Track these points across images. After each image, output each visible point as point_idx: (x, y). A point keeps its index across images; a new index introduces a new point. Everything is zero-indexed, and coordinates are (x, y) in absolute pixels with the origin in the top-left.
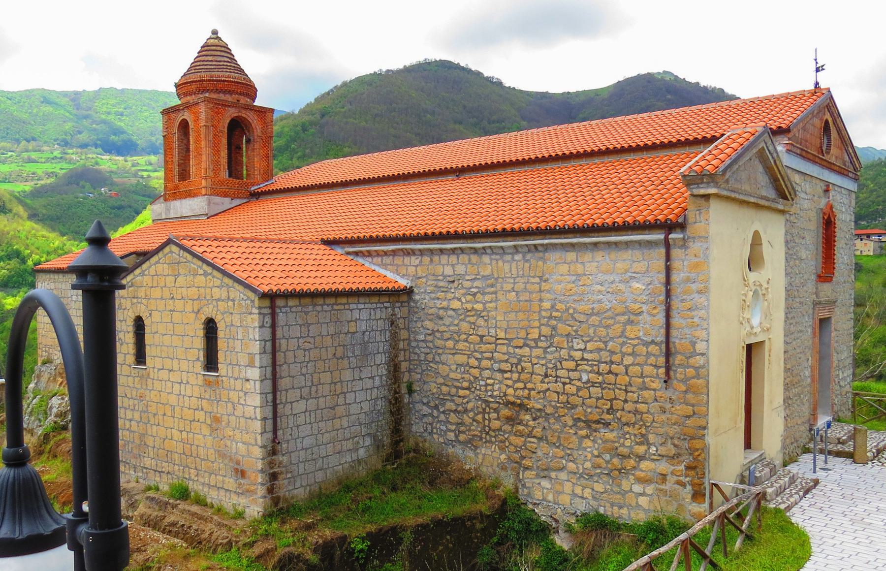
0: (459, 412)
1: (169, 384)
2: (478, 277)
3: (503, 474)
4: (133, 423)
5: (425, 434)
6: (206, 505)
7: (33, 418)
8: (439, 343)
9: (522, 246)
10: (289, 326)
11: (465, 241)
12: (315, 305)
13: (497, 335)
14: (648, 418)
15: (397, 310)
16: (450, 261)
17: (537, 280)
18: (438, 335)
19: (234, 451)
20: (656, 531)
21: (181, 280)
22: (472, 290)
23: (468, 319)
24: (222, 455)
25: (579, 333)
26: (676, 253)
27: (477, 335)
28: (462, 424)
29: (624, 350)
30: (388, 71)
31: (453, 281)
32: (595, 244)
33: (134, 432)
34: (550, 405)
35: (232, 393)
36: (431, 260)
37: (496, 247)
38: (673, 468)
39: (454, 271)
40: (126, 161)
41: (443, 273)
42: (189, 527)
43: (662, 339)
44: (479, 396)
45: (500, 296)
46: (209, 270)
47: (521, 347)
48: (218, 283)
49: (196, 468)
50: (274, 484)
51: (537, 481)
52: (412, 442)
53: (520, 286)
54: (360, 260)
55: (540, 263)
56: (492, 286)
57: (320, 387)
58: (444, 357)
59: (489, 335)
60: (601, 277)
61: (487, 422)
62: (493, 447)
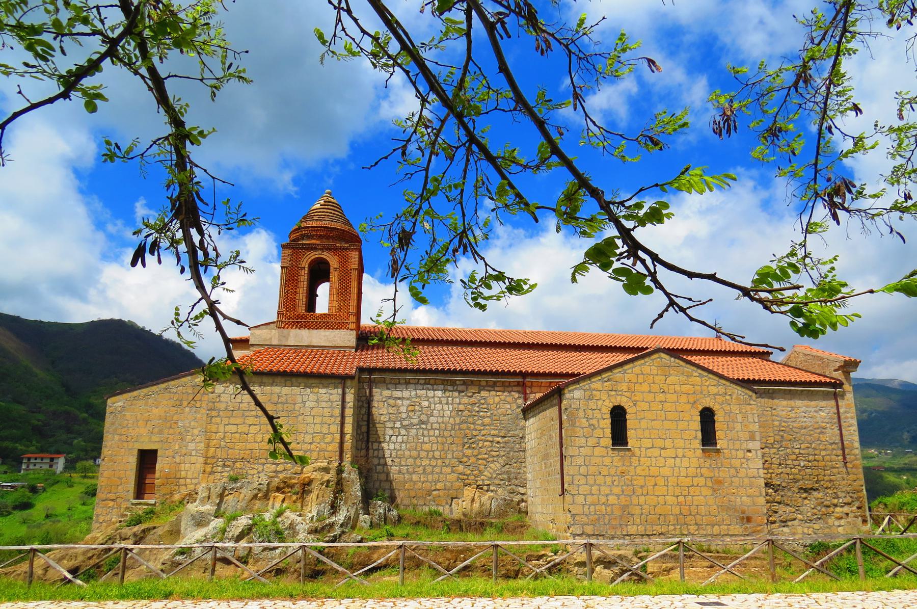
4: (610, 498)
14: (837, 483)
24: (728, 508)
35: (733, 461)
49: (696, 524)
51: (781, 529)
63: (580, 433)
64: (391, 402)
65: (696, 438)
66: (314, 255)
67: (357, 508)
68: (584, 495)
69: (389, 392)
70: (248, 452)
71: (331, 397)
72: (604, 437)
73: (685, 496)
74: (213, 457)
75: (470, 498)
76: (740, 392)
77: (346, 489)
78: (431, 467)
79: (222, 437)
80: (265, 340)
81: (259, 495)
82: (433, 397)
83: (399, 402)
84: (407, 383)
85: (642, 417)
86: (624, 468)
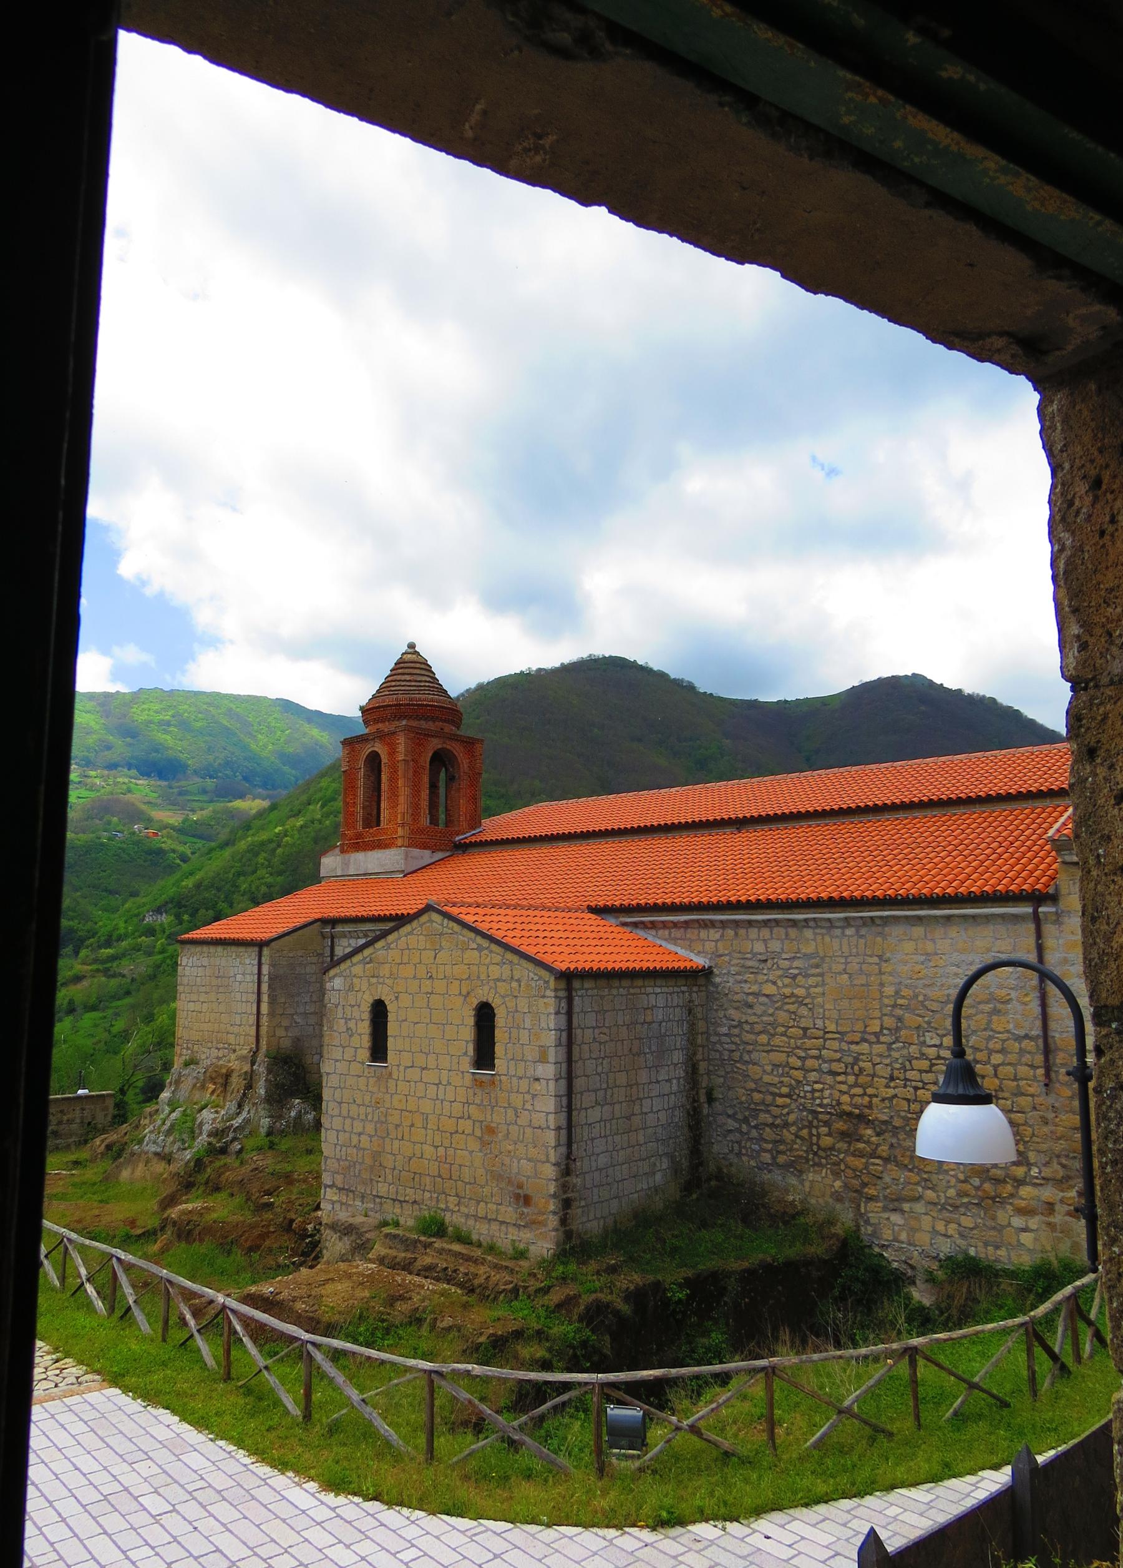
0: (777, 1126)
1: (421, 1086)
2: (798, 955)
3: (838, 1206)
4: (363, 1137)
5: (731, 1156)
6: (471, 1243)
7: (171, 1138)
8: (750, 1037)
9: (854, 918)
10: (586, 1013)
11: (780, 911)
12: (611, 987)
13: (826, 1028)
15: (694, 995)
16: (761, 935)
17: (876, 960)
18: (747, 1027)
19: (515, 1170)
20: (1046, 1277)
21: (443, 956)
23: (787, 1007)
25: (932, 1025)
26: (1049, 929)
27: (799, 1027)
28: (782, 1141)
29: (991, 1045)
30: (540, 670)
31: (766, 961)
32: (948, 918)
33: (364, 1149)
34: (899, 1116)
35: (513, 1096)
36: (736, 934)
37: (821, 919)
38: (1062, 1194)
39: (766, 948)
40: (171, 788)
41: (752, 950)
42: (455, 1271)
43: (1037, 1033)
44: (803, 1105)
45: (828, 980)
46: (485, 943)
47: (857, 1043)
48: (498, 959)
49: (457, 1195)
50: (567, 1213)
51: (886, 1215)
52: (712, 1167)
53: (854, 966)
54: (641, 933)
55: (879, 939)
56: (817, 966)
57: (616, 1090)
58: (755, 1055)
59: (815, 1028)
60: (956, 957)
61: (815, 1139)
62: (824, 1171)
70: (201, 1034)
73: (446, 1147)
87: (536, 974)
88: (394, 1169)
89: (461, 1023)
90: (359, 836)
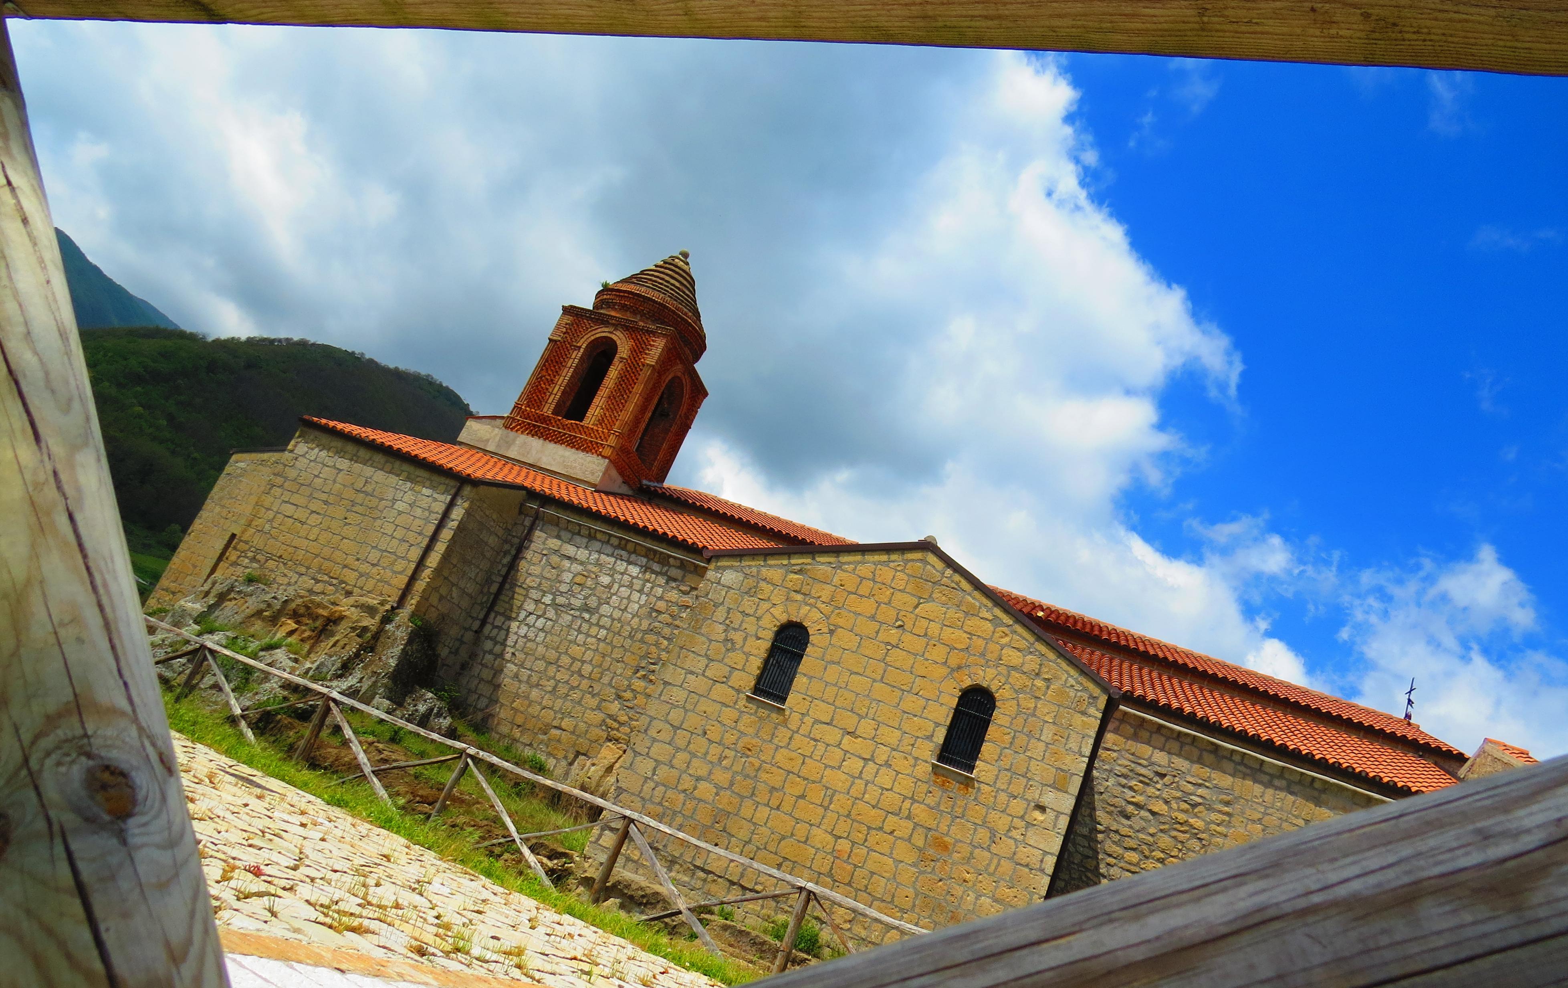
2: (1207, 784)
4: (702, 785)
18: (1116, 838)
22: (1193, 797)
35: (993, 816)
56: (1227, 803)
63: (702, 648)
64: (555, 559)
65: (930, 738)
66: (602, 332)
67: (375, 682)
68: (656, 760)
69: (559, 543)
70: (291, 550)
71: (434, 504)
72: (743, 670)
74: (246, 542)
75: (606, 763)
76: (1072, 681)
77: (379, 649)
78: (567, 687)
79: (271, 517)
80: (480, 440)
81: (265, 614)
82: (622, 574)
83: (566, 563)
84: (592, 537)
85: (836, 659)
86: (755, 741)
87: (1081, 684)
88: (749, 842)
89: (935, 698)
90: (544, 419)
